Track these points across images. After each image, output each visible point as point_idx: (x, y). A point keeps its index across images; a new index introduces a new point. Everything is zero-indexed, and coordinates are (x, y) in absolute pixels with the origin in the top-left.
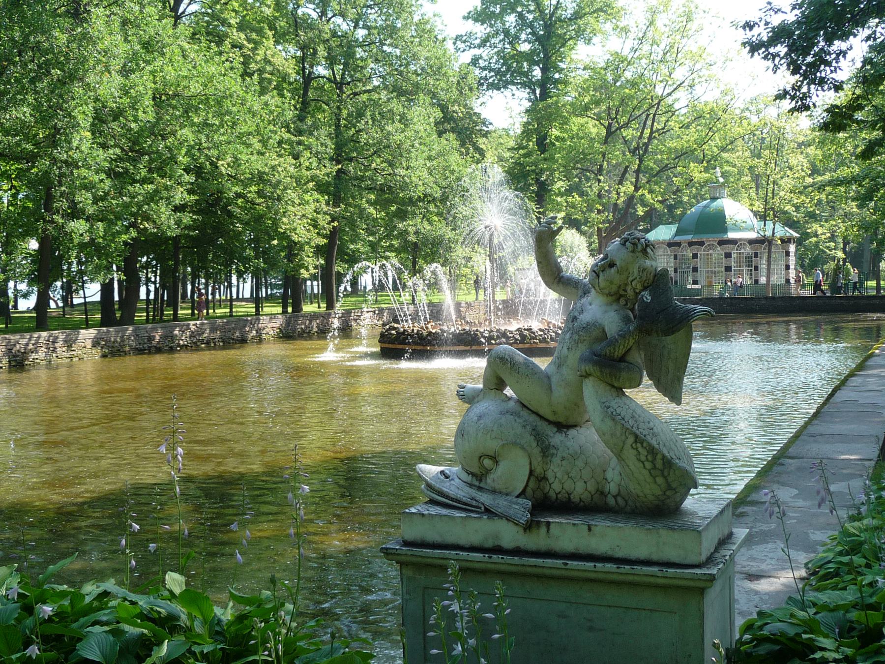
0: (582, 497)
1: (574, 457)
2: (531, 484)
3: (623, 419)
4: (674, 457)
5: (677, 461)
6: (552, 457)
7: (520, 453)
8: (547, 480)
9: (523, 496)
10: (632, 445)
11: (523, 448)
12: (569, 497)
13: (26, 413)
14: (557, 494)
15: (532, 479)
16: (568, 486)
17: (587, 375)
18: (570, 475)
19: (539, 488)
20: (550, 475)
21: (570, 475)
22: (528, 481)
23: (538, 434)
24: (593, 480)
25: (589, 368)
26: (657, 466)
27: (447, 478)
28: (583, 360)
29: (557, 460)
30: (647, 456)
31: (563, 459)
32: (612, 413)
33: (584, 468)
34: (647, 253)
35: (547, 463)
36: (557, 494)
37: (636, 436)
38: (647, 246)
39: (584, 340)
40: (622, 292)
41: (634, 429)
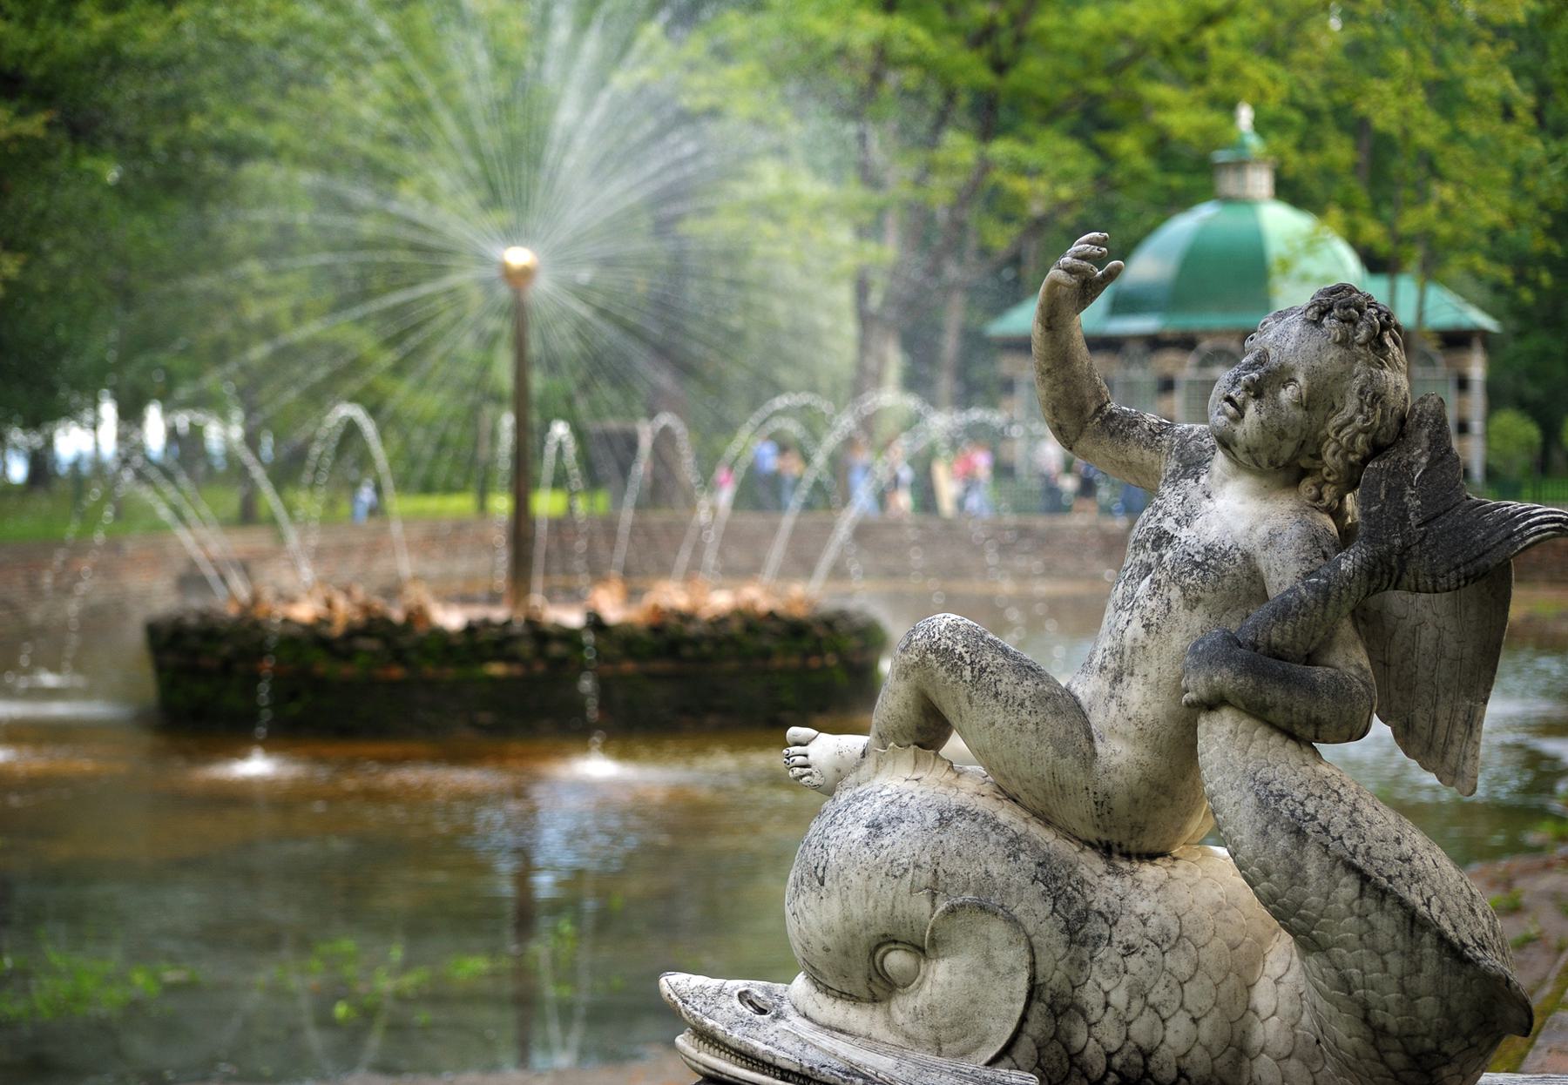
0: (1185, 1063)
1: (1168, 942)
2: (1035, 1027)
3: (1326, 829)
4: (1470, 942)
5: (1479, 954)
6: (1096, 946)
7: (997, 930)
8: (1083, 1013)
9: (1007, 1061)
10: (1349, 906)
11: (1012, 920)
12: (1146, 1065)
13: (1557, 525)
14: (1109, 1055)
15: (1039, 1008)
16: (1141, 1030)
17: (1212, 704)
18: (1152, 999)
19: (1055, 1037)
20: (1090, 997)
21: (1152, 999)
22: (1024, 1019)
23: (1056, 879)
24: (1216, 1010)
25: (1224, 678)
26: (1043, 997)
27: (762, 1012)
28: (1204, 654)
29: (1108, 955)
30: (1393, 937)
31: (1130, 950)
32: (1293, 813)
33: (1191, 978)
34: (1383, 345)
35: (1082, 964)
36: (1109, 1055)
37: (1364, 878)
38: (1384, 327)
39: (1198, 600)
40: (1305, 462)
41: (1359, 861)
